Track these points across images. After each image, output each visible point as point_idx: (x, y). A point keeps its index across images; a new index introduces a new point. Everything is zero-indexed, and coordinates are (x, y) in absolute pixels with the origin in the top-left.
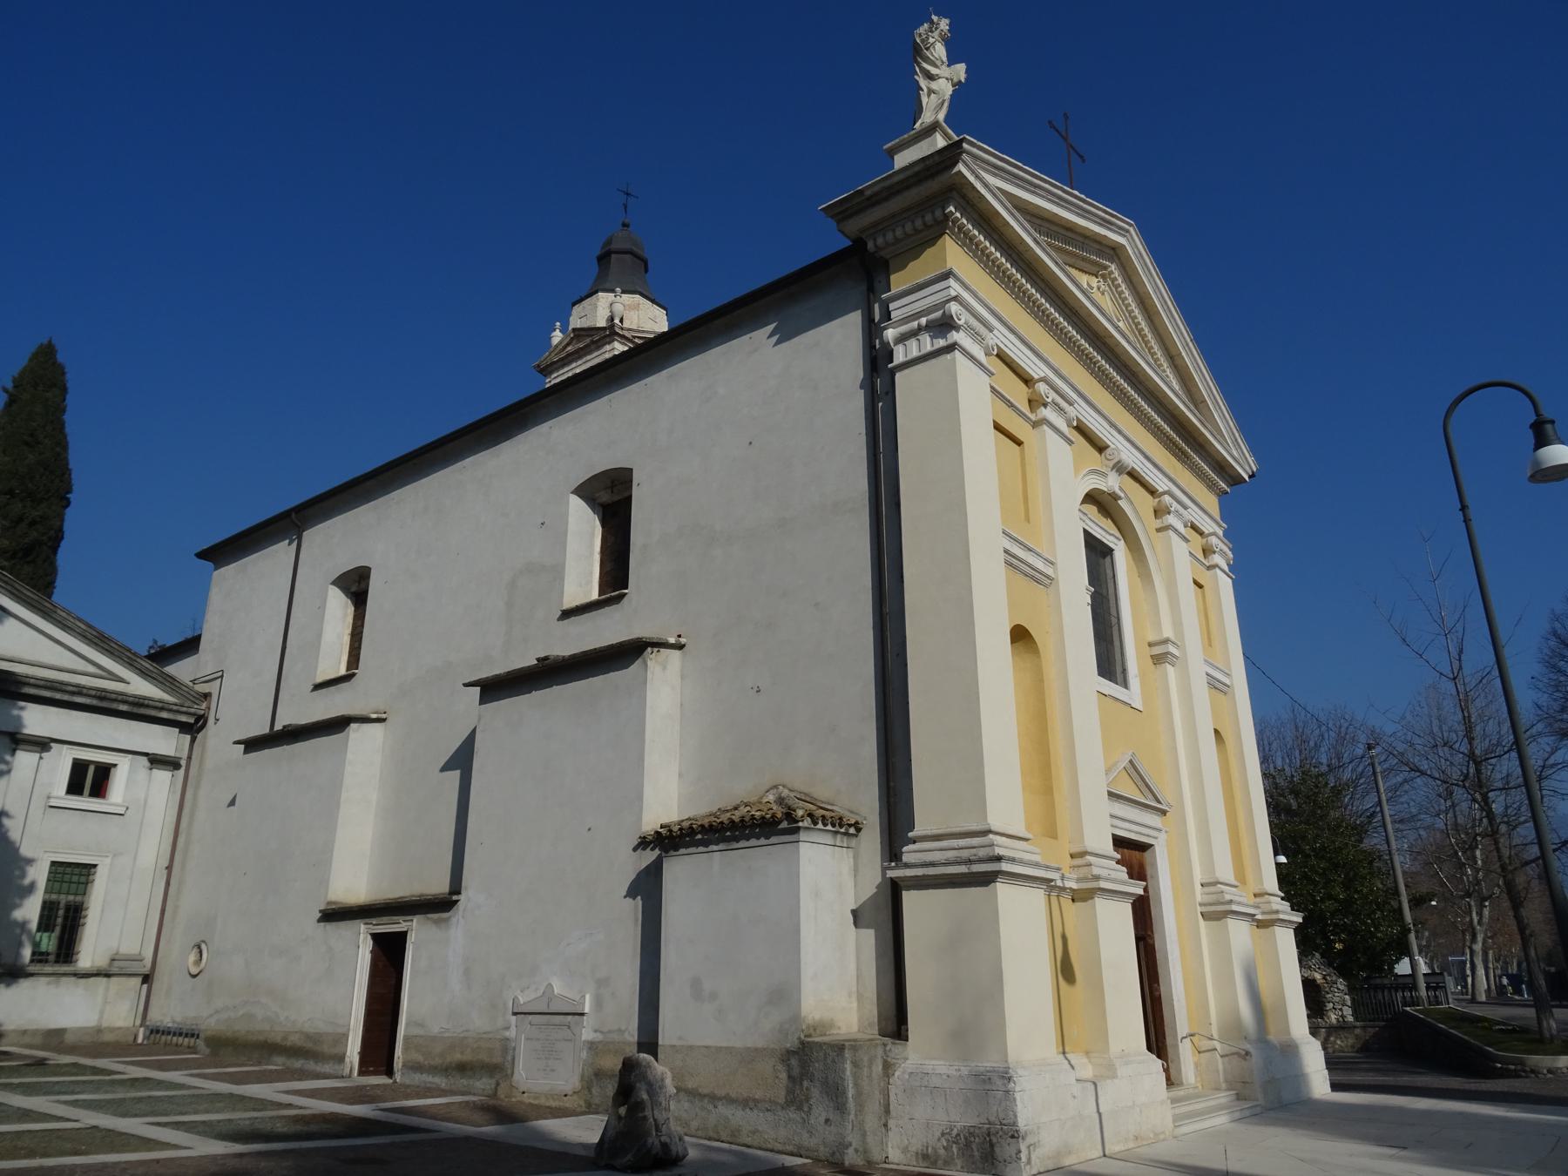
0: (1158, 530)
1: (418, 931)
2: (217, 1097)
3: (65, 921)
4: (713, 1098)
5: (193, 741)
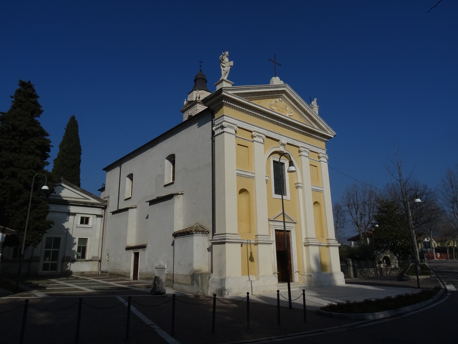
0: (299, 156)
1: (140, 251)
2: (104, 284)
3: (83, 250)
4: (181, 284)
5: (105, 211)
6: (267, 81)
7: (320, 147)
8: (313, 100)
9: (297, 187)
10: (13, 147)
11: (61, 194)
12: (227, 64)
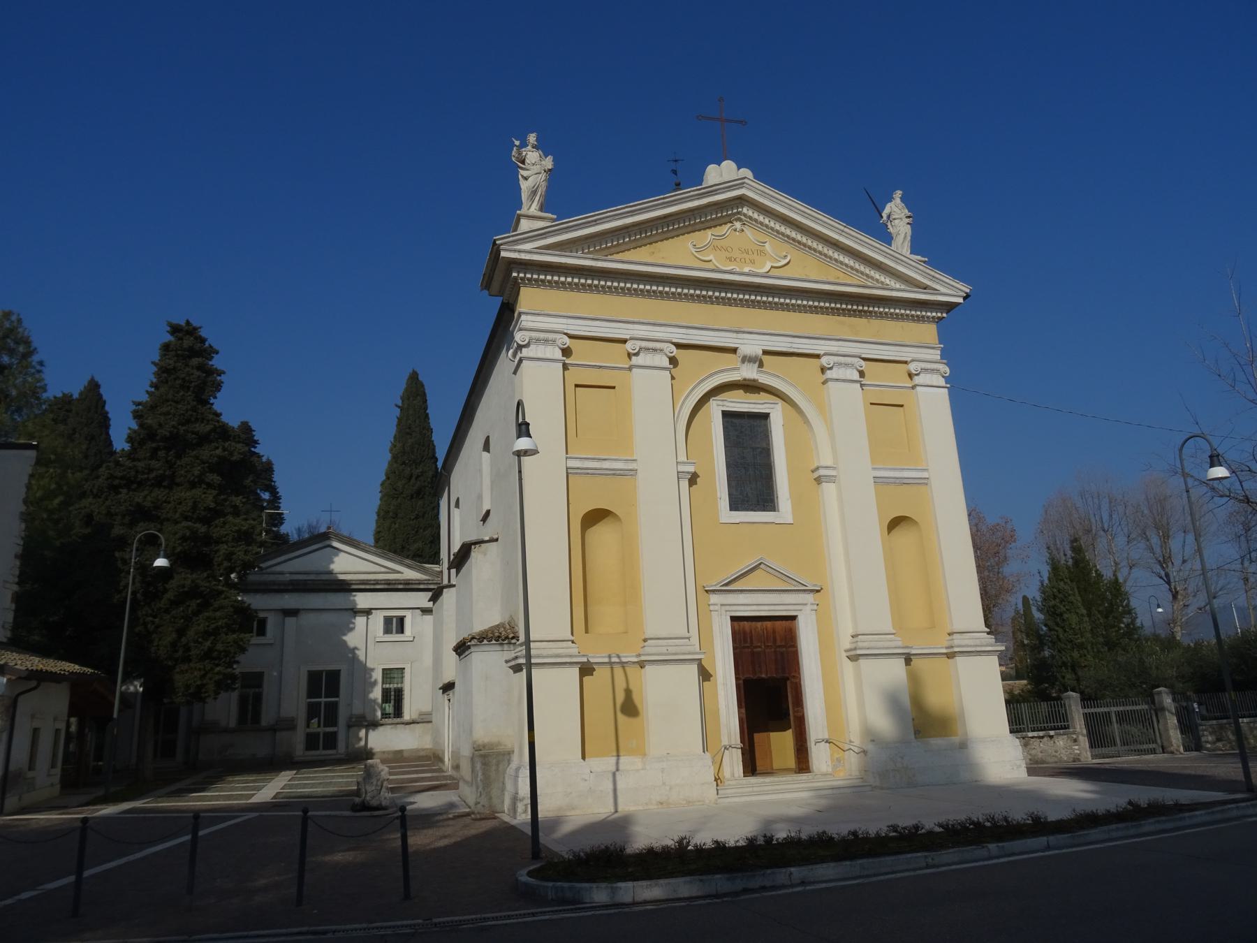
0: (824, 383)
3: (395, 698)
6: (698, 179)
7: (919, 343)
8: (890, 199)
9: (818, 480)
10: (152, 475)
11: (332, 567)
12: (536, 169)
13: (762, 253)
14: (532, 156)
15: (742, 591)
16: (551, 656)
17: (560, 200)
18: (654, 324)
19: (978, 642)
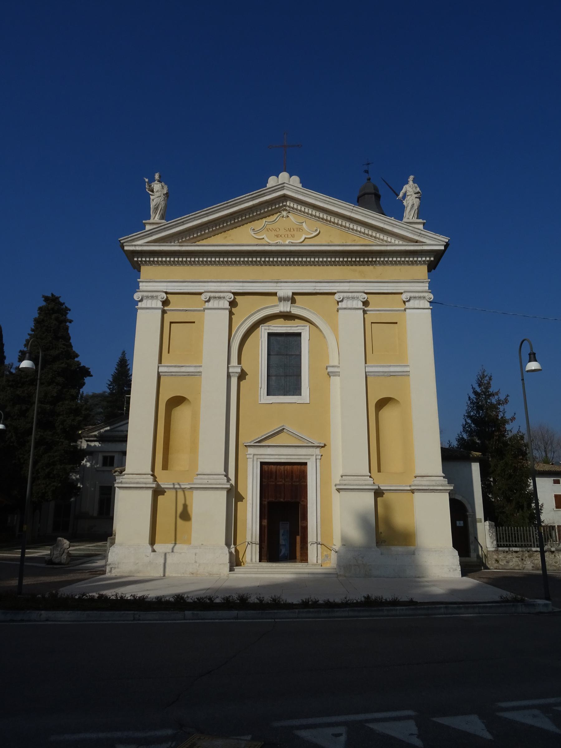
7: (414, 282)
8: (407, 183)
13: (300, 229)
14: (157, 186)
15: (269, 446)
16: (134, 483)
17: (170, 212)
18: (221, 282)
19: (434, 483)
